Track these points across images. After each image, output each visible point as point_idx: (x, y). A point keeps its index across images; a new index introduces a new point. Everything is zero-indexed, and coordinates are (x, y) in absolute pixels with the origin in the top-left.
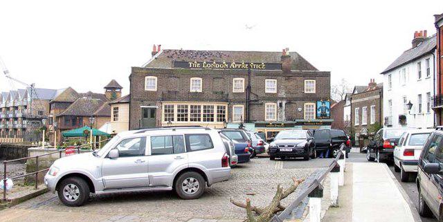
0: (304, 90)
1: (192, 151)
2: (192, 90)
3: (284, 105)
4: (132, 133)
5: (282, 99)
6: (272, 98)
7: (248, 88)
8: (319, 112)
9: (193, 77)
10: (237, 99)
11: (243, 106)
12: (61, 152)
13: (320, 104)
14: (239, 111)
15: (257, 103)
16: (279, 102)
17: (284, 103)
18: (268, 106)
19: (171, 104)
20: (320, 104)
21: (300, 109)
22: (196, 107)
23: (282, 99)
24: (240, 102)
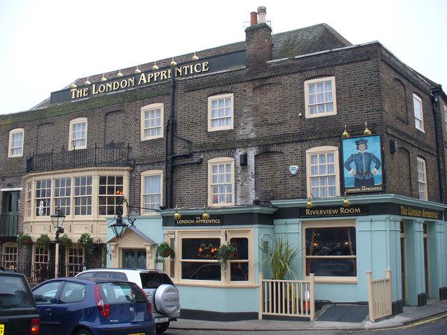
0: (303, 110)
3: (251, 161)
5: (246, 143)
6: (224, 144)
7: (171, 126)
8: (350, 174)
13: (350, 147)
14: (153, 184)
15: (189, 161)
16: (239, 153)
17: (252, 154)
18: (314, 156)
21: (294, 169)
22: (111, 179)
23: (246, 143)
24: (153, 164)
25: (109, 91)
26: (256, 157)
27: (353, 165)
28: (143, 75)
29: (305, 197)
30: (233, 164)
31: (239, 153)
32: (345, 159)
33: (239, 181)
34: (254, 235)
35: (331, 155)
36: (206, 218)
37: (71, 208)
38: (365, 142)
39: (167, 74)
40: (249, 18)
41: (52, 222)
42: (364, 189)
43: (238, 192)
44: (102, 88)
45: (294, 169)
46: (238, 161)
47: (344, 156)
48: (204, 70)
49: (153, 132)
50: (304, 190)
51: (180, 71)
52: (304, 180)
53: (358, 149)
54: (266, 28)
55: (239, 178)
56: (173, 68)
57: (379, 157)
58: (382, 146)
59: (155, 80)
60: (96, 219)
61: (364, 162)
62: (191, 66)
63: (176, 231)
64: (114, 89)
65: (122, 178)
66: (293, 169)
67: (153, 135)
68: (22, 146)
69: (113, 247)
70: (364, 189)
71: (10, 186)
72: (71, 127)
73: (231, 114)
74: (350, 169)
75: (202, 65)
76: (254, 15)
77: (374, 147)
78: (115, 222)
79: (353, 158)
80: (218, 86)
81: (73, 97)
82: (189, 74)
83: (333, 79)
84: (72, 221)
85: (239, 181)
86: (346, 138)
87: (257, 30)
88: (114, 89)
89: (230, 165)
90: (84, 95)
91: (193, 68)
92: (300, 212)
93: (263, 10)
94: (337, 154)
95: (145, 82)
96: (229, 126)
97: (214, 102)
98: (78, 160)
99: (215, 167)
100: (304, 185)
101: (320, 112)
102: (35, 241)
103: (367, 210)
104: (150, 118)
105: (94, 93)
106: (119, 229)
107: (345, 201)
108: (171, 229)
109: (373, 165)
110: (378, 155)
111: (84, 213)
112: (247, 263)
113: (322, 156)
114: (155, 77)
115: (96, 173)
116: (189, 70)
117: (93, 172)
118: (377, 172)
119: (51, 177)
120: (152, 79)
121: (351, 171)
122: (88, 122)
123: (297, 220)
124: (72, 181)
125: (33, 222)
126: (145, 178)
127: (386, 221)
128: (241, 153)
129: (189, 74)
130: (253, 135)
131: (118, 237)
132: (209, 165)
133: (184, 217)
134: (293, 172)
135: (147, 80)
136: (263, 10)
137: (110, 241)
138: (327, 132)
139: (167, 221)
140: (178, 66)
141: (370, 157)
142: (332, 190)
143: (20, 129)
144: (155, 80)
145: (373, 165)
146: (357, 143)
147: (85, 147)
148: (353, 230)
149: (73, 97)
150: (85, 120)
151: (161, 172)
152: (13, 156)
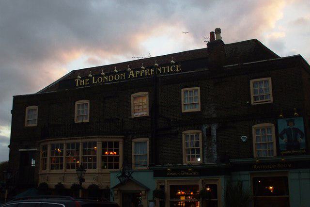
0: (249, 100)
1: (45, 191)
2: (186, 110)
3: (214, 132)
4: (97, 169)
6: (194, 121)
7: (154, 106)
8: (283, 142)
9: (272, 80)
10: (140, 127)
11: (147, 139)
12: (248, 181)
13: (283, 125)
14: (141, 148)
16: (205, 127)
17: (214, 128)
18: (257, 130)
19: (77, 141)
20: (283, 125)
21: (244, 138)
24: (142, 134)
25: (122, 80)
26: (217, 130)
27: (285, 136)
28: (132, 72)
29: (252, 157)
30: (200, 135)
31: (205, 127)
32: (280, 132)
33: (205, 146)
34: (221, 183)
35: (269, 129)
36: (190, 172)
37: (64, 164)
38: (293, 121)
39: (150, 72)
40: (209, 36)
41: (77, 174)
42: (293, 151)
43: (205, 153)
44: (100, 80)
45: (244, 138)
46: (205, 133)
47: (279, 129)
48: (177, 70)
49: (195, 106)
50: (252, 152)
51: (160, 70)
52: (252, 145)
53: (288, 125)
54: (220, 42)
55: (205, 144)
56: (155, 68)
57: (303, 131)
58: (304, 123)
59: (141, 75)
60: (100, 172)
61: (292, 134)
62: (168, 67)
63: (166, 181)
64: (110, 80)
65: (96, 143)
66: (244, 138)
67: (32, 124)
68: (36, 118)
69: (116, 192)
70: (293, 151)
71: (27, 147)
72: (76, 106)
73: (198, 101)
74: (283, 139)
75: (176, 67)
76: (212, 34)
77: (300, 124)
78: (121, 174)
79: (285, 131)
80: (190, 82)
81: (77, 85)
82: (162, 73)
83: (270, 79)
84: (65, 174)
85: (205, 146)
86: (281, 118)
87: (215, 42)
88: (110, 80)
89: (199, 135)
90: (86, 84)
91: (170, 69)
92: (248, 167)
93: (218, 31)
94: (273, 129)
95: (134, 76)
96: (198, 109)
97: (185, 92)
98: (82, 130)
99: (187, 136)
100: (252, 149)
101: (190, 109)
102: (54, 187)
103: (296, 165)
104: (81, 109)
105: (93, 83)
106: (123, 179)
107: (283, 160)
108: (161, 179)
109: (299, 135)
110: (302, 129)
111: (57, 168)
112: (217, 201)
113: (263, 130)
114: (141, 73)
115: (100, 140)
116: (166, 69)
117: (97, 139)
118: (302, 141)
119: (80, 141)
120: (139, 75)
121: (284, 140)
122: (90, 103)
123: (248, 172)
124: (81, 145)
125: (49, 174)
126: (136, 143)
127: (248, 175)
128: (206, 127)
129: (162, 73)
130: (214, 116)
131: (122, 184)
132: (183, 135)
133: (173, 170)
134: (244, 141)
135: (135, 75)
136: (218, 31)
137: (115, 187)
138: (266, 113)
139: (157, 174)
140: (158, 67)
141: (297, 130)
142: (271, 151)
143: (86, 101)
144: (141, 75)
145: (299, 135)
146: (288, 122)
147: (88, 121)
148: (286, 179)
149: (77, 85)
150: (87, 102)
151: (148, 139)
152: (28, 125)
